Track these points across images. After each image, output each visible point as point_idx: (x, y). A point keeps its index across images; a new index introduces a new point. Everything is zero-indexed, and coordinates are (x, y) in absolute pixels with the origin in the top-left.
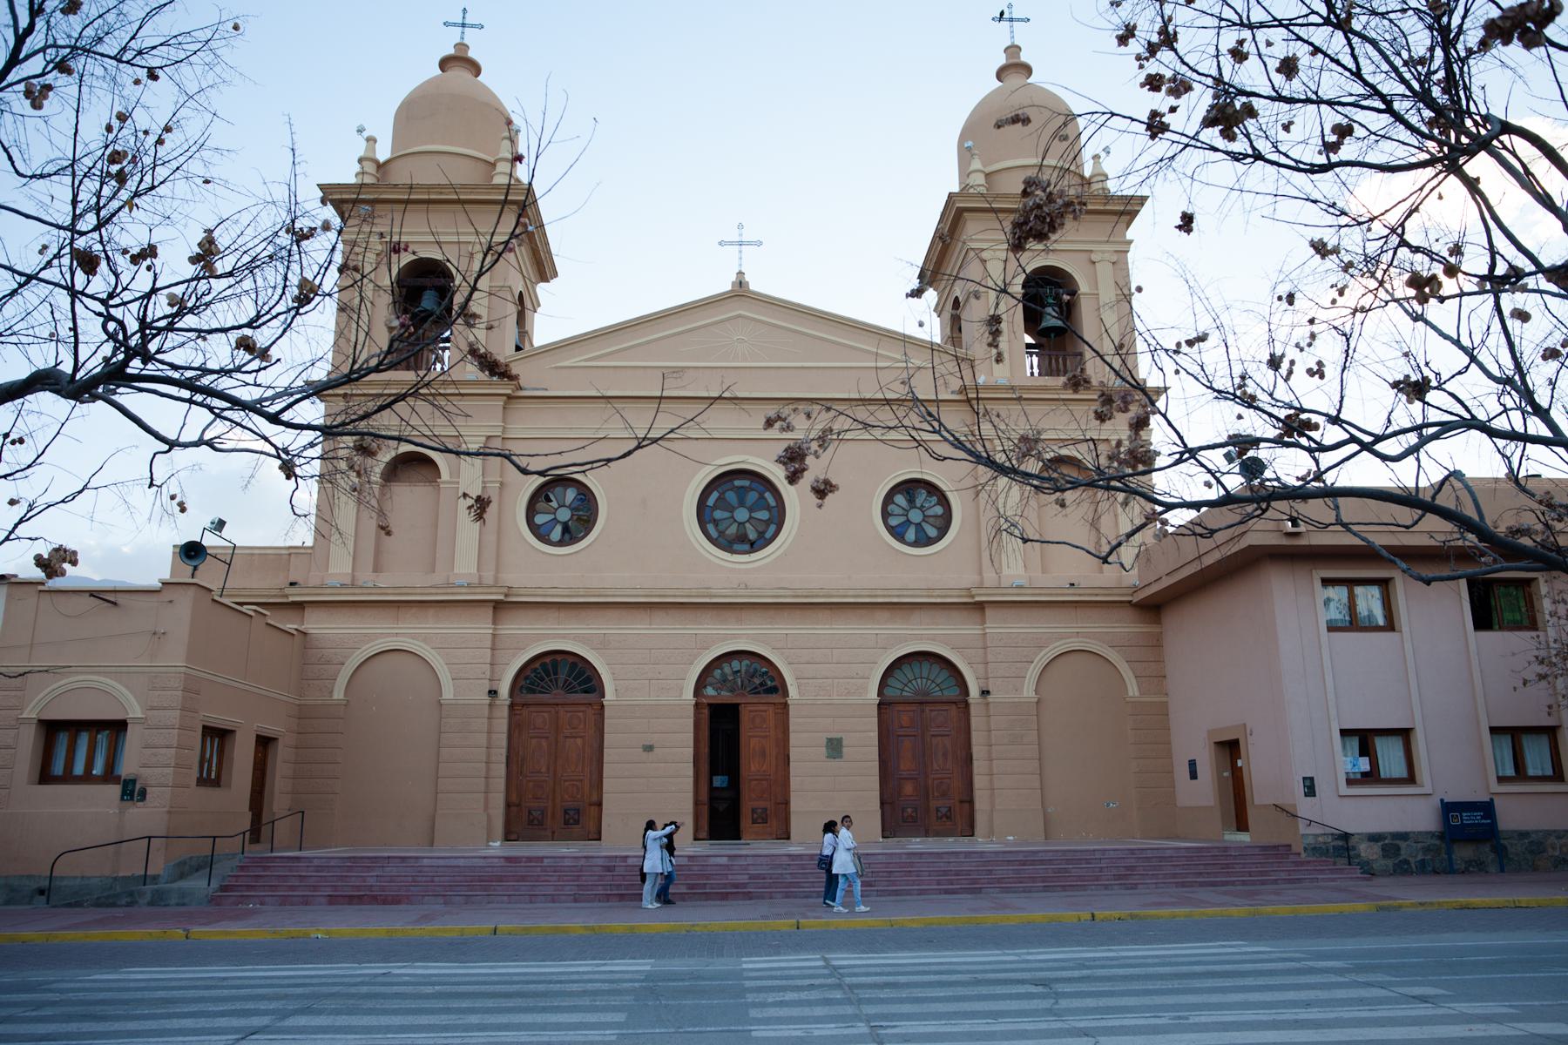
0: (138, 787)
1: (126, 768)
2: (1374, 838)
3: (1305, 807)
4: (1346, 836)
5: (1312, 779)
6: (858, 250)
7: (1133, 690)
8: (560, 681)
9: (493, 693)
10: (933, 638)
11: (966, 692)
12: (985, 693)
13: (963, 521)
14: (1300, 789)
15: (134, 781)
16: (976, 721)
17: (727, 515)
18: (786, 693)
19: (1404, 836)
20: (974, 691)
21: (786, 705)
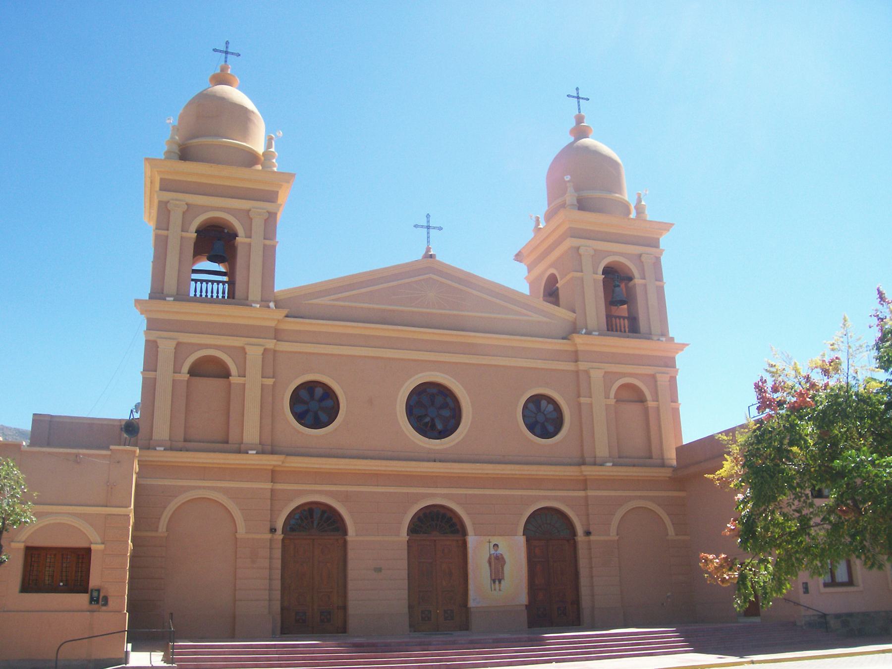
0: (102, 595)
1: (94, 582)
2: (837, 616)
3: (804, 599)
4: (824, 616)
5: (806, 583)
6: (495, 242)
7: (671, 531)
8: (316, 525)
9: (273, 530)
10: (556, 498)
11: (574, 533)
12: (588, 533)
13: (283, 399)
14: (801, 590)
15: (99, 591)
16: (582, 552)
17: (546, 424)
18: (345, 532)
19: (850, 615)
20: (580, 530)
21: (345, 542)
